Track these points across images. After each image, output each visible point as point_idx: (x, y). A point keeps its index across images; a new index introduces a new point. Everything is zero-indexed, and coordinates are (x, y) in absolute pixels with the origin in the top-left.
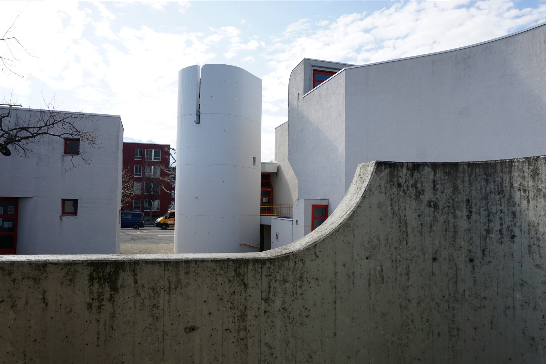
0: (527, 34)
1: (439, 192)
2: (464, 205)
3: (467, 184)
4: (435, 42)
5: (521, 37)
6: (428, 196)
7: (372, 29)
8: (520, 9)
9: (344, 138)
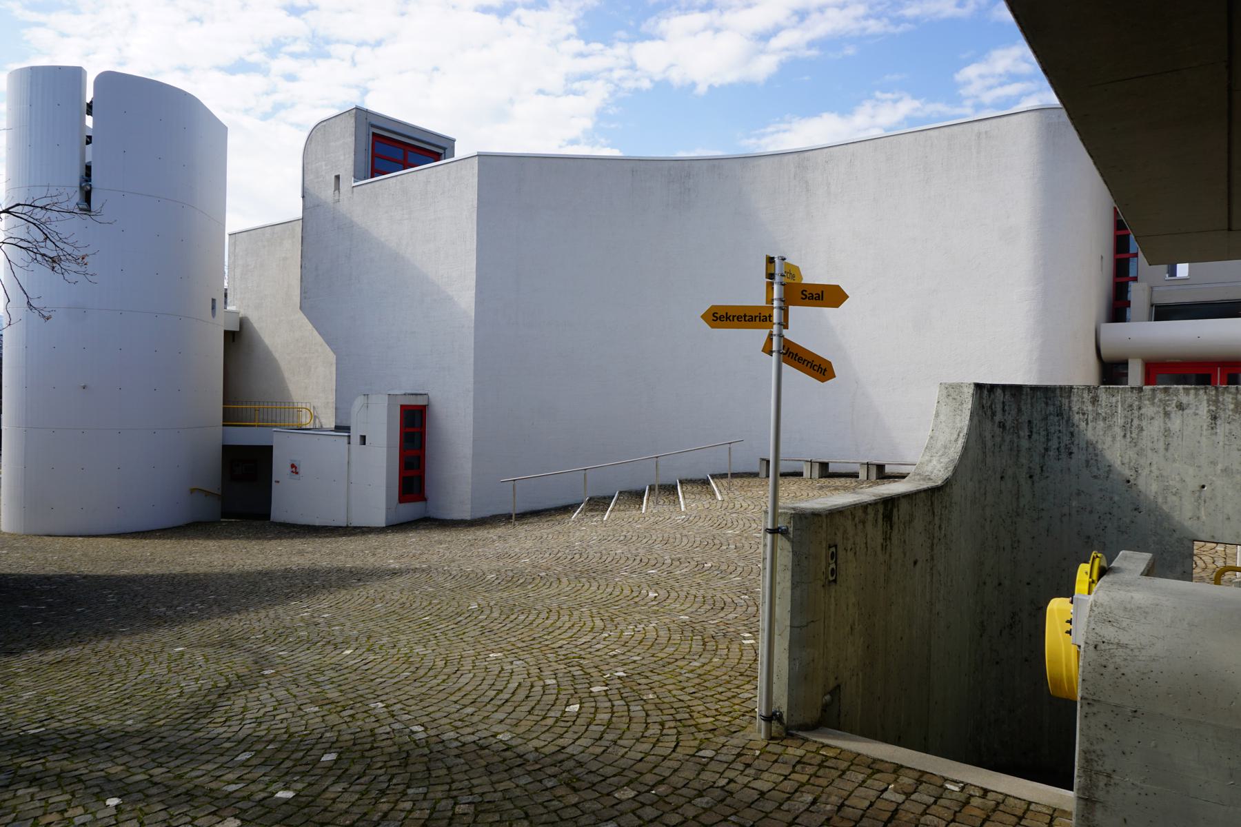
0: (772, 159)
1: (1007, 413)
2: (1026, 426)
3: (1029, 406)
4: (436, 69)
5: (763, 161)
6: (998, 418)
7: (306, 10)
8: (587, 43)
9: (473, 283)
